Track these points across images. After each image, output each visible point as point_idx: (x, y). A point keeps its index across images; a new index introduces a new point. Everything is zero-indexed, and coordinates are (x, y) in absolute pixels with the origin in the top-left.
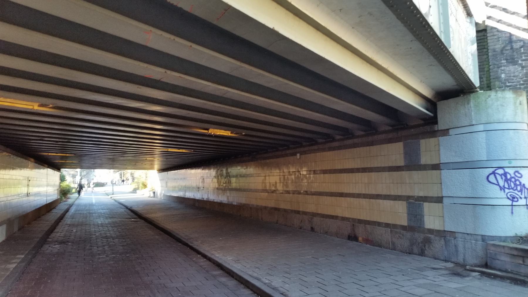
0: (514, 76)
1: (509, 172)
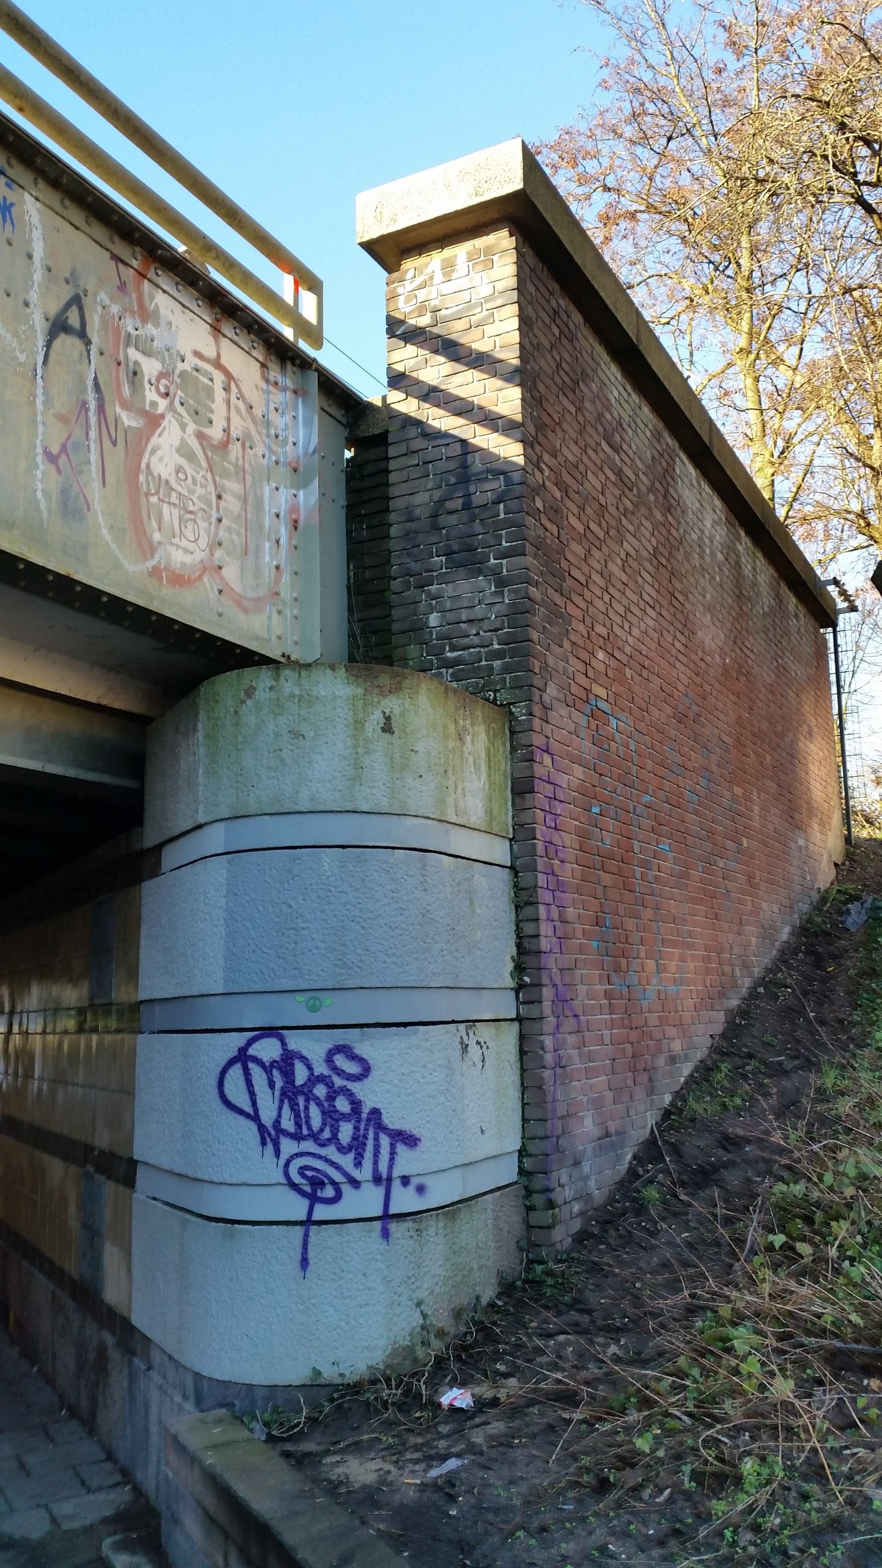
0: (470, 621)
1: (305, 1053)
